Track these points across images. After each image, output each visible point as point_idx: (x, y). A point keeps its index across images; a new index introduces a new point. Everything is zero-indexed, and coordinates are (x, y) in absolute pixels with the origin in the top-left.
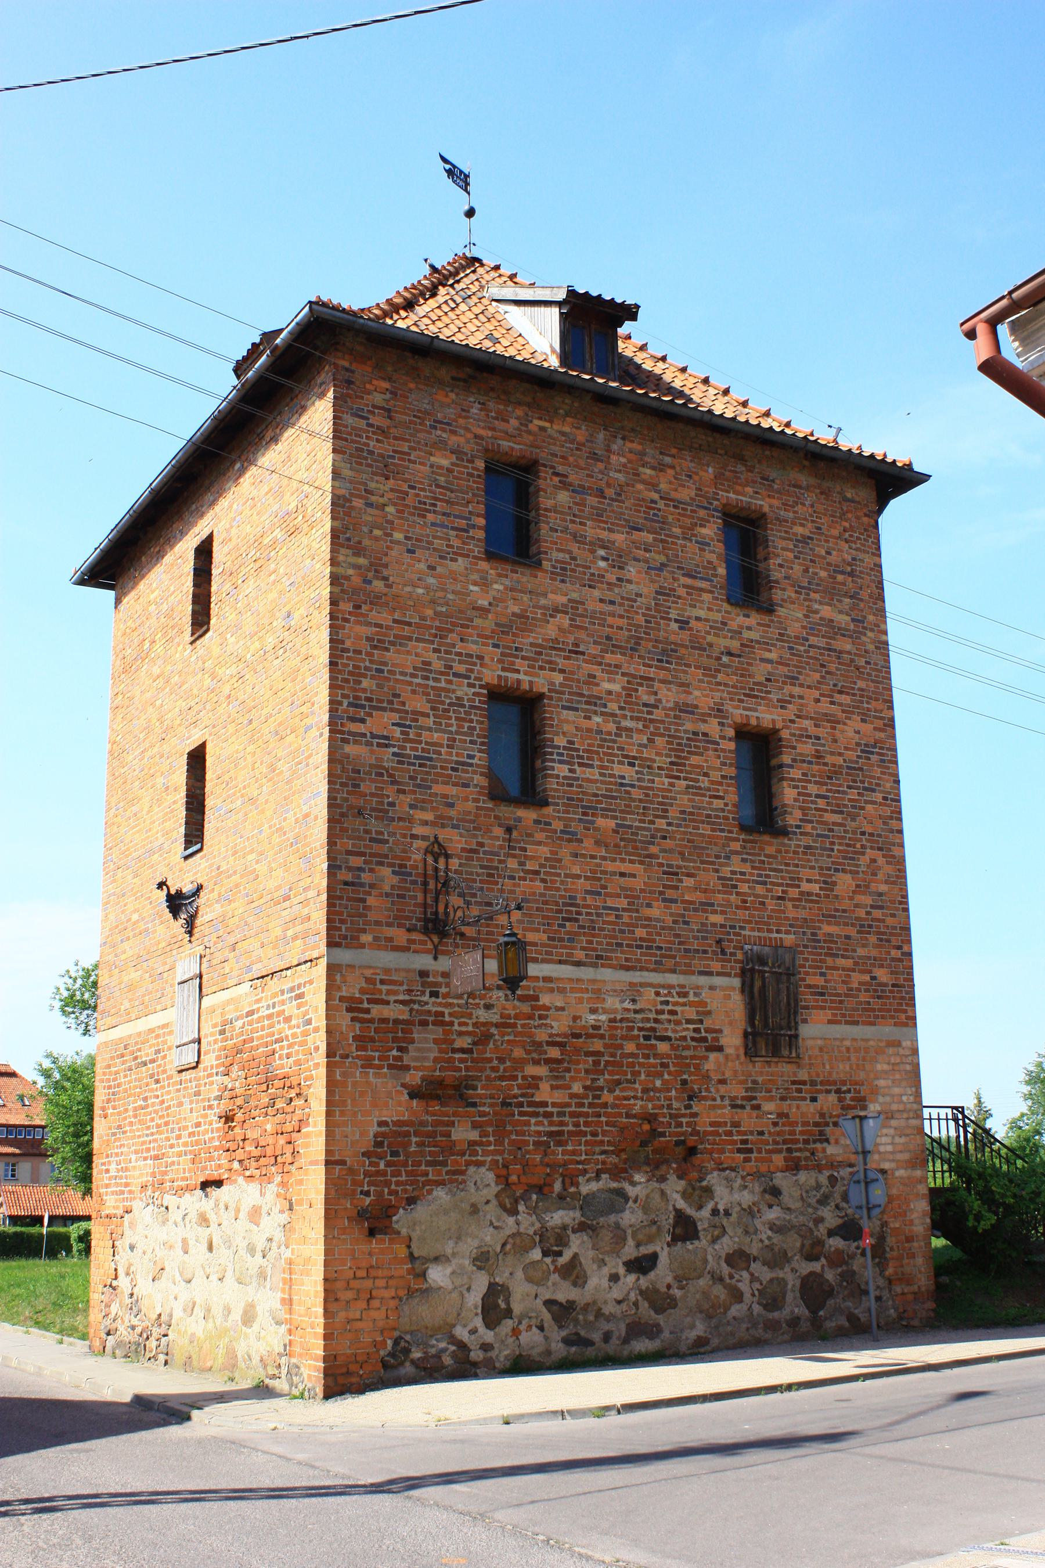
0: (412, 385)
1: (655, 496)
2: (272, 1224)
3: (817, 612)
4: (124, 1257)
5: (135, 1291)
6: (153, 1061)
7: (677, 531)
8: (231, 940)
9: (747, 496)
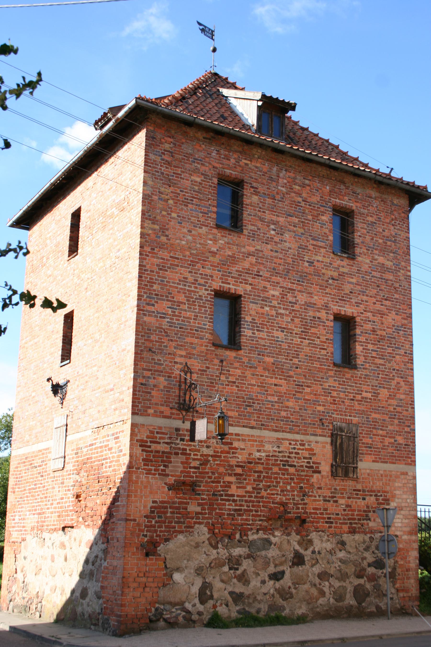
0: (184, 141)
1: (300, 199)
6: (40, 466)
7: (310, 217)
9: (346, 202)
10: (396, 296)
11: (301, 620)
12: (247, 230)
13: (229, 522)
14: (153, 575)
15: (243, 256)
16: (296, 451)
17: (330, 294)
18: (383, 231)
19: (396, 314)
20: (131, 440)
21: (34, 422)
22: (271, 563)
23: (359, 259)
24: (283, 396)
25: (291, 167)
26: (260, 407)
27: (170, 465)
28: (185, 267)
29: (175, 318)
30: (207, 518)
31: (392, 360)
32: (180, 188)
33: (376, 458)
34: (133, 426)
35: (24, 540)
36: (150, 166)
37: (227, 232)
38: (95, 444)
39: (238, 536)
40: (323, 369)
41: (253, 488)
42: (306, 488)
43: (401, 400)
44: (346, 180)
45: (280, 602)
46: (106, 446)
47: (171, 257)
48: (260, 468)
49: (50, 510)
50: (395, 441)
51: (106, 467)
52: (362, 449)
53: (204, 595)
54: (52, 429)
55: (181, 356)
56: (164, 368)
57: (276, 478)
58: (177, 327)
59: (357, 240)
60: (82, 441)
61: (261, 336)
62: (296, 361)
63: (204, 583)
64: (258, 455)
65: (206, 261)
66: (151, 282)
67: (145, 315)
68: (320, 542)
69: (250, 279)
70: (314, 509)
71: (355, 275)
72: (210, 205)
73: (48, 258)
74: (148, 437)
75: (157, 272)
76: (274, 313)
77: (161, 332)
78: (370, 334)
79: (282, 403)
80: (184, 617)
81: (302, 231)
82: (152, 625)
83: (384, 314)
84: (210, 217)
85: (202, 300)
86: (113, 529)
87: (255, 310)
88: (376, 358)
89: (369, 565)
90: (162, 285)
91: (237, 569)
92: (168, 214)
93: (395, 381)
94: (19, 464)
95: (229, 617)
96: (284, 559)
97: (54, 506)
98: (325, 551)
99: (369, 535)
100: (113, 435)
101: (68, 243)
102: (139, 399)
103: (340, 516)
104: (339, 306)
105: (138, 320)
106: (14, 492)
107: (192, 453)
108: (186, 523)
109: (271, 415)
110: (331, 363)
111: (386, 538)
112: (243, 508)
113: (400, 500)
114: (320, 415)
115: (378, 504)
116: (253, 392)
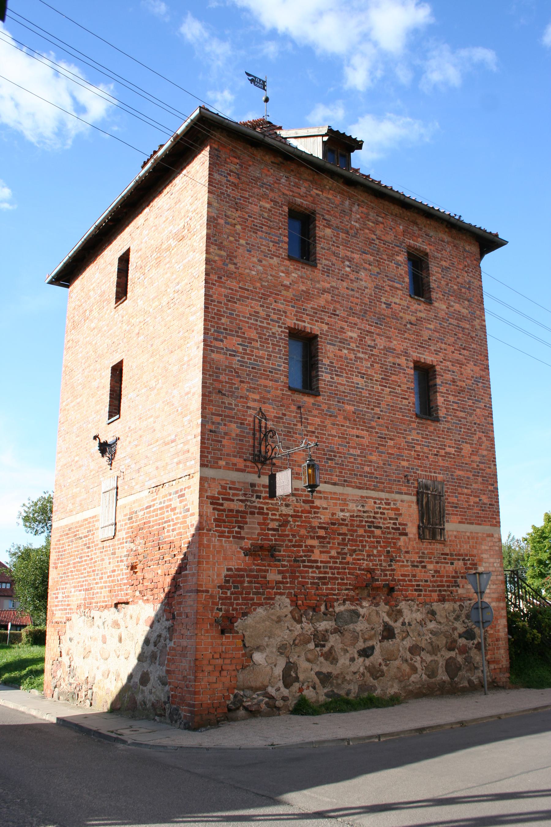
0: (251, 163)
1: (374, 237)
3: (452, 306)
7: (385, 257)
9: (420, 244)
10: (474, 346)
11: (394, 701)
13: (313, 591)
14: (230, 656)
15: (318, 293)
16: (381, 510)
17: (409, 340)
18: (458, 277)
19: (475, 365)
20: (201, 496)
21: (78, 489)
22: (360, 638)
23: (436, 304)
24: (365, 449)
25: (363, 202)
26: (342, 461)
27: (245, 526)
28: (256, 300)
29: (246, 356)
30: (289, 588)
31: (472, 414)
33: (462, 519)
34: (203, 480)
35: (69, 620)
36: (215, 187)
37: (300, 265)
38: (154, 505)
39: (323, 608)
40: (405, 420)
41: (338, 553)
42: (393, 552)
43: (483, 456)
44: (419, 221)
45: (371, 681)
46: (167, 507)
47: (240, 288)
48: (344, 530)
50: (480, 500)
51: (168, 531)
52: (449, 509)
53: (289, 677)
54: (99, 494)
55: (255, 400)
56: (236, 414)
57: (361, 541)
58: (249, 367)
59: (433, 285)
60: (136, 504)
61: (340, 381)
62: (377, 410)
63: (288, 663)
64: (341, 514)
65: (278, 295)
66: (219, 315)
67: (212, 351)
68: (410, 612)
69: (326, 318)
70: (402, 575)
71: (432, 321)
72: (280, 234)
73: (91, 311)
74: (219, 493)
75: (225, 304)
76: (352, 356)
77: (232, 372)
78: (450, 384)
79: (365, 457)
80: (267, 704)
81: (378, 270)
82: (231, 715)
83: (463, 365)
84: (282, 248)
85: (276, 338)
86: (180, 603)
87: (333, 352)
88: (457, 410)
89: (460, 636)
90: (231, 318)
91: (324, 646)
92: (236, 240)
93: (477, 436)
94: (61, 536)
95: (317, 701)
96: (373, 632)
97: (104, 580)
98: (415, 622)
99: (458, 603)
100: (176, 492)
101: (115, 289)
102: (208, 448)
103: (429, 583)
104: (418, 353)
105: (204, 357)
106: (56, 568)
107: (270, 513)
108: (265, 594)
109: (353, 470)
110: (413, 414)
111: (480, 606)
112: (327, 575)
113: (487, 565)
114: (405, 471)
115: (466, 569)
116: (334, 444)
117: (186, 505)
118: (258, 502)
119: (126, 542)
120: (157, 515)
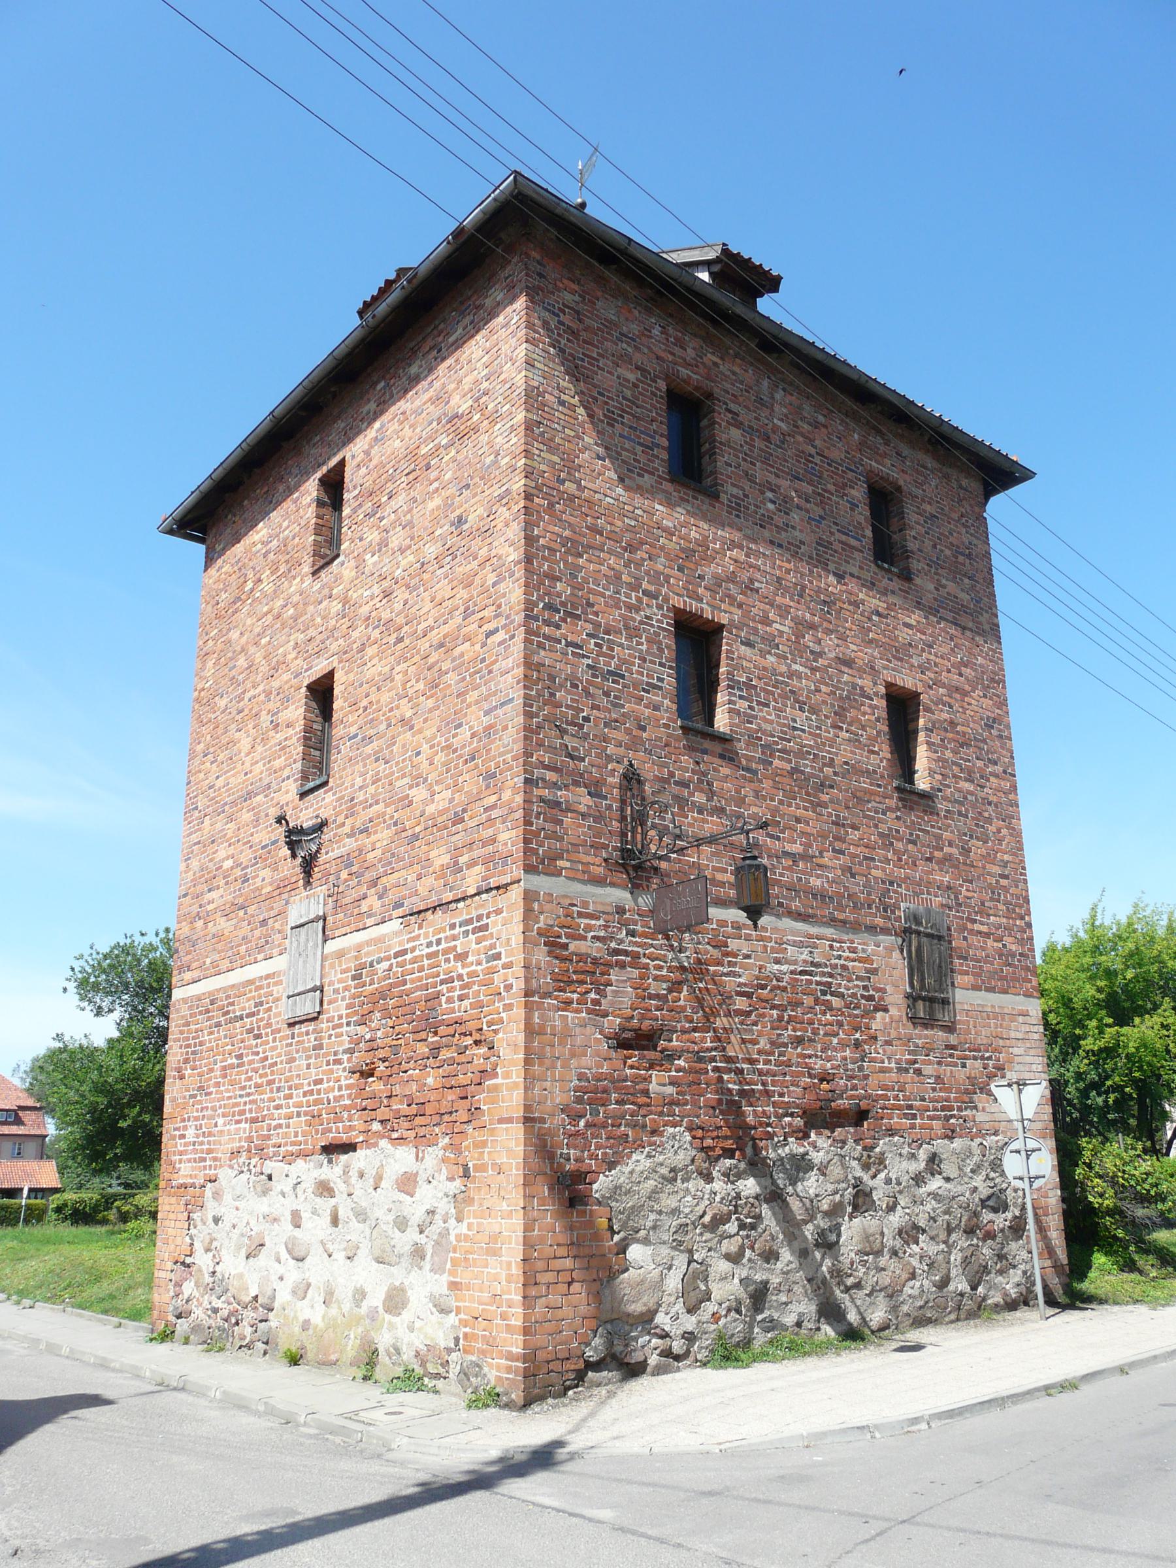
0: (599, 294)
1: (813, 451)
2: (438, 1190)
3: (944, 587)
4: (201, 1233)
5: (218, 1268)
6: (252, 1015)
7: (831, 487)
8: (370, 875)
9: (888, 468)
12: (726, 493)
14: (587, 1251)
16: (842, 962)
23: (918, 581)
32: (599, 386)
38: (413, 950)
41: (772, 1043)
46: (446, 952)
49: (284, 1111)
67: (541, 646)
97: (295, 1099)
106: (182, 1078)
117: (493, 946)
118: (630, 942)
119: (348, 1024)
120: (421, 969)
